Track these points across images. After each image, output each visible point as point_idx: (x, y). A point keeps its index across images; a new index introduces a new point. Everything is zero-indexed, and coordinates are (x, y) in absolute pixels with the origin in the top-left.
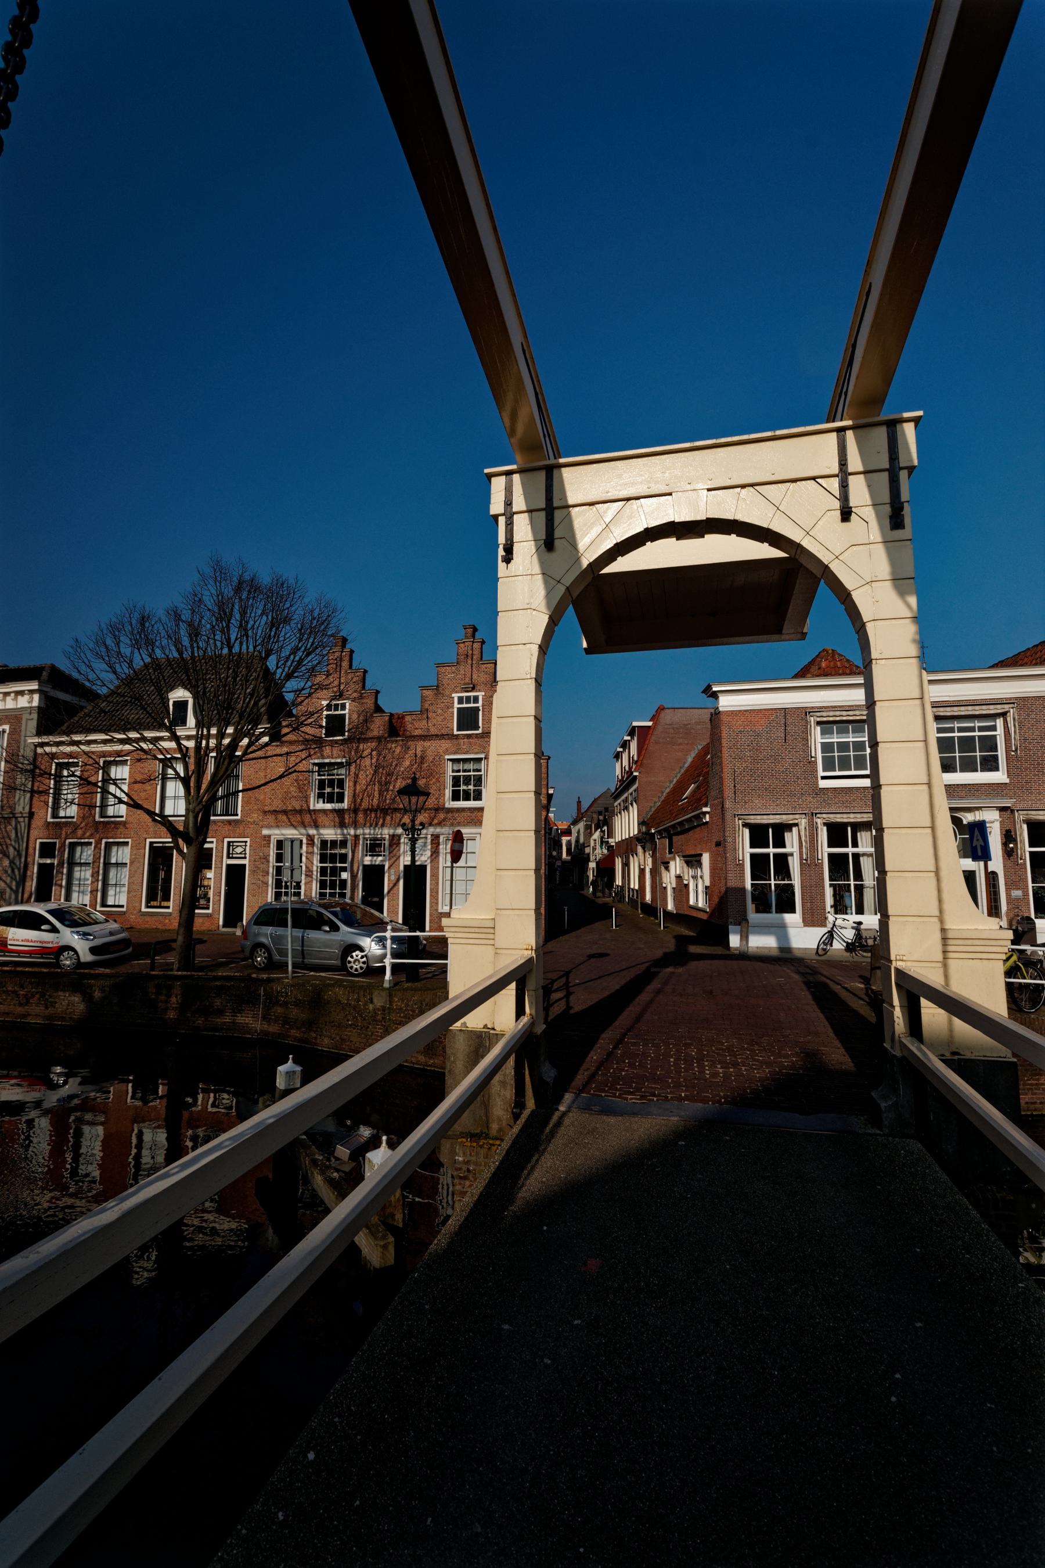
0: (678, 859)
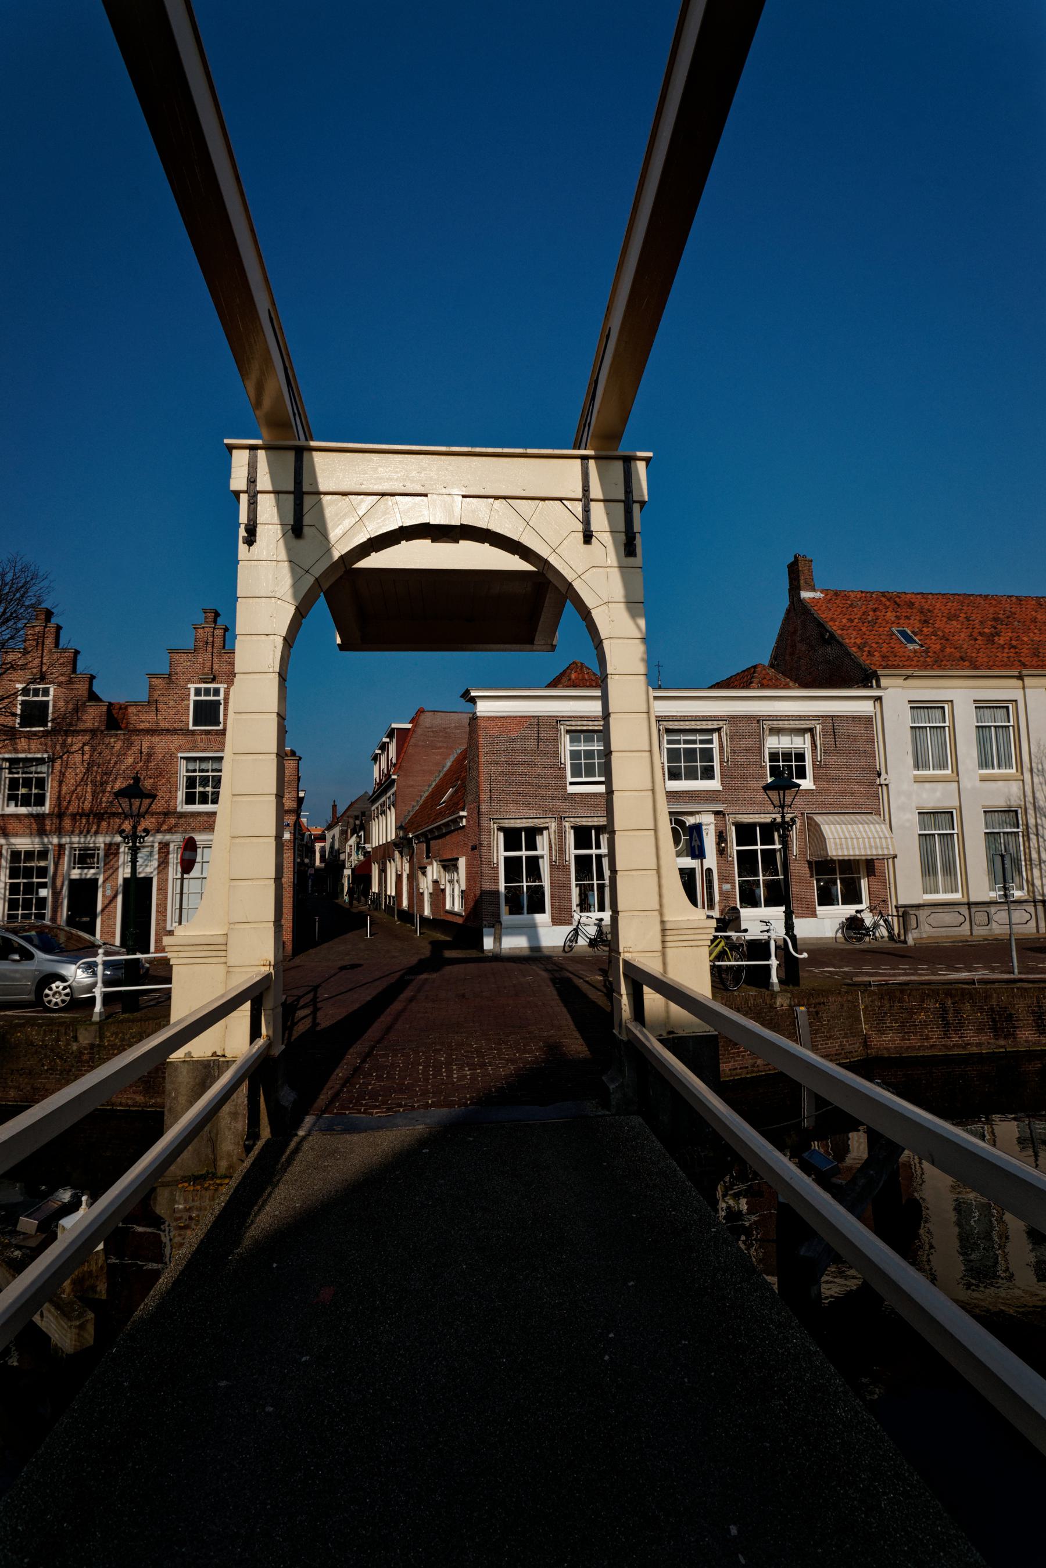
0: (435, 864)
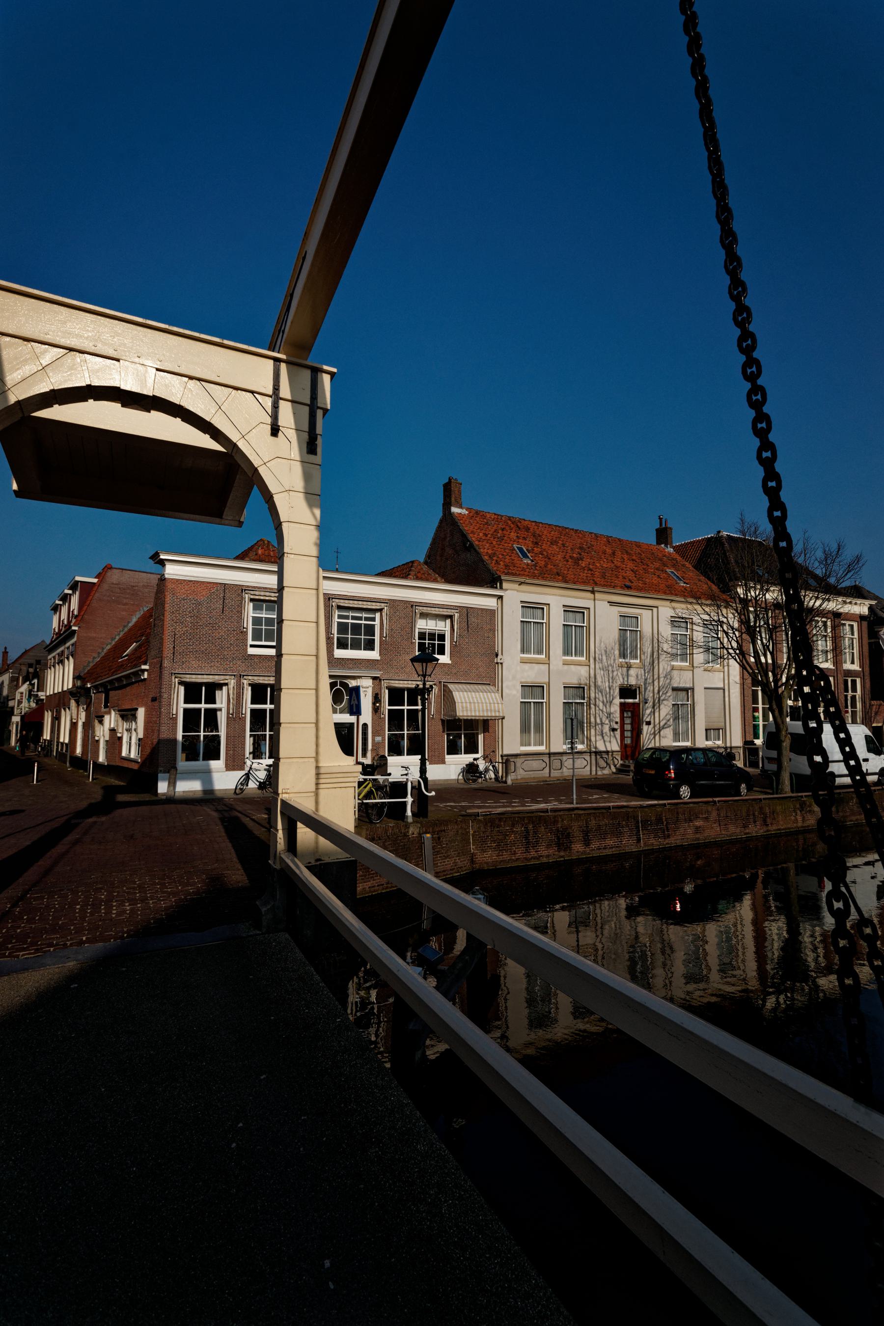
0: (113, 713)
